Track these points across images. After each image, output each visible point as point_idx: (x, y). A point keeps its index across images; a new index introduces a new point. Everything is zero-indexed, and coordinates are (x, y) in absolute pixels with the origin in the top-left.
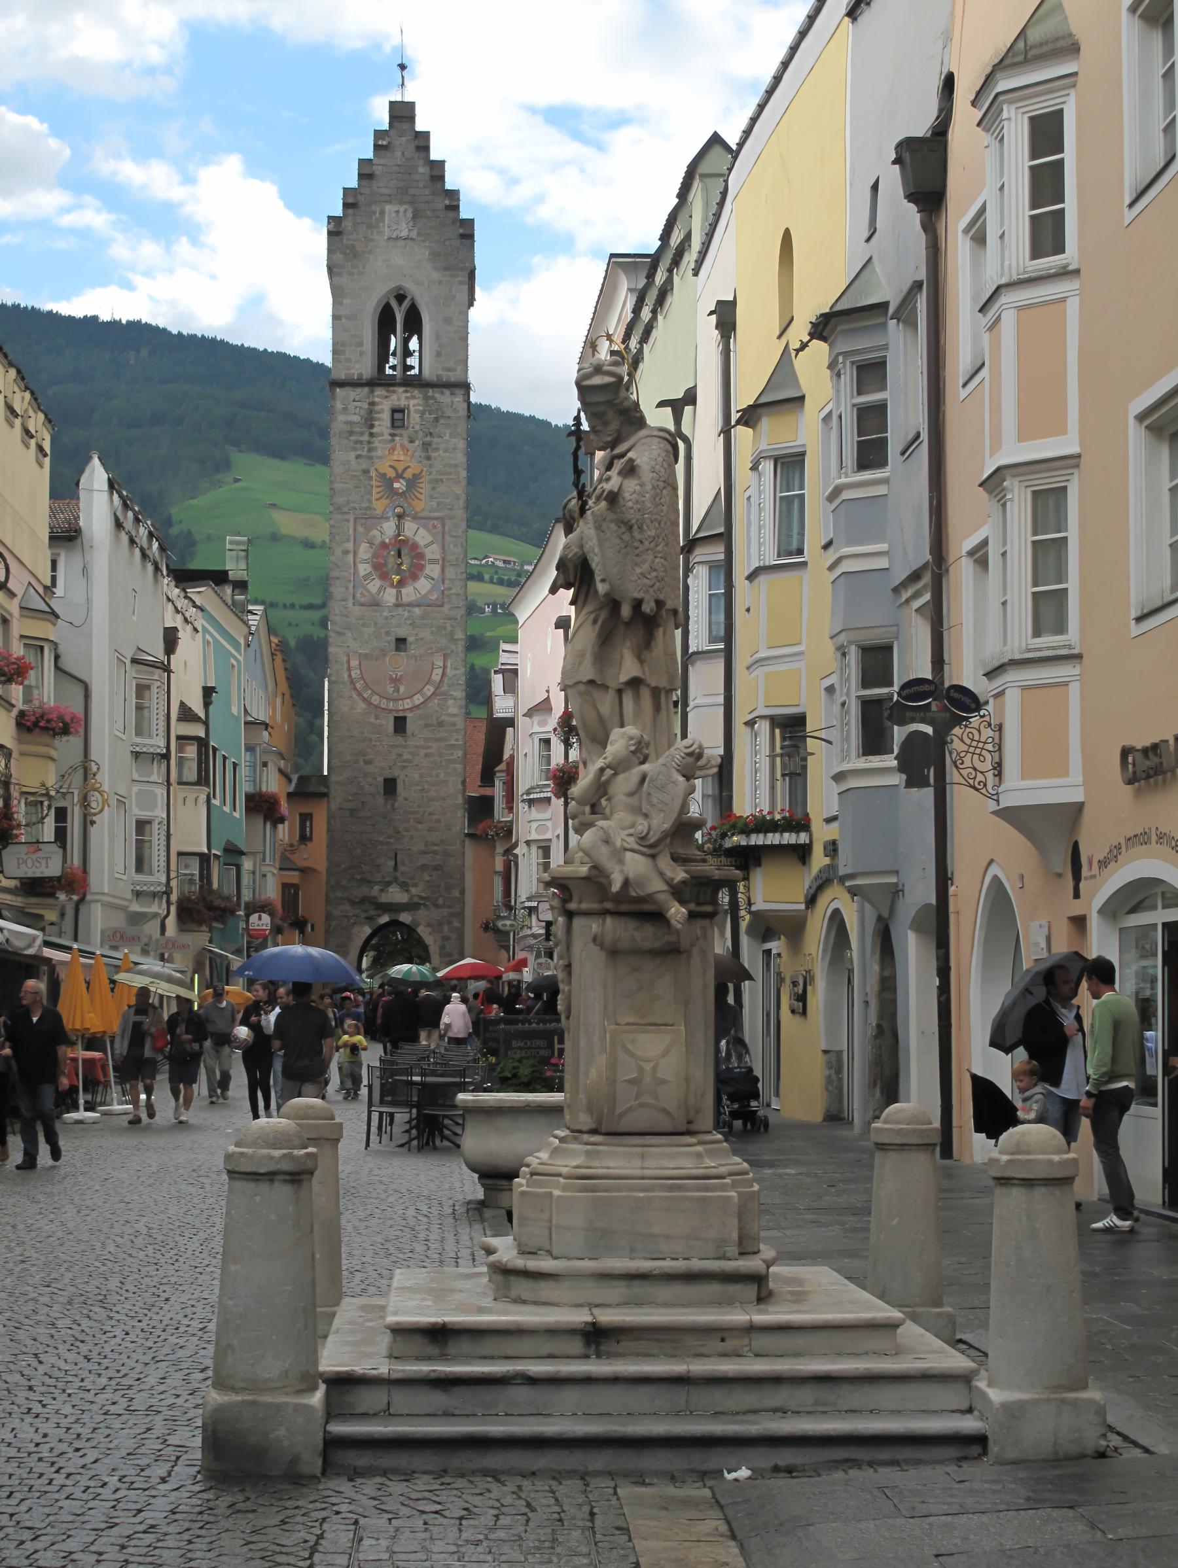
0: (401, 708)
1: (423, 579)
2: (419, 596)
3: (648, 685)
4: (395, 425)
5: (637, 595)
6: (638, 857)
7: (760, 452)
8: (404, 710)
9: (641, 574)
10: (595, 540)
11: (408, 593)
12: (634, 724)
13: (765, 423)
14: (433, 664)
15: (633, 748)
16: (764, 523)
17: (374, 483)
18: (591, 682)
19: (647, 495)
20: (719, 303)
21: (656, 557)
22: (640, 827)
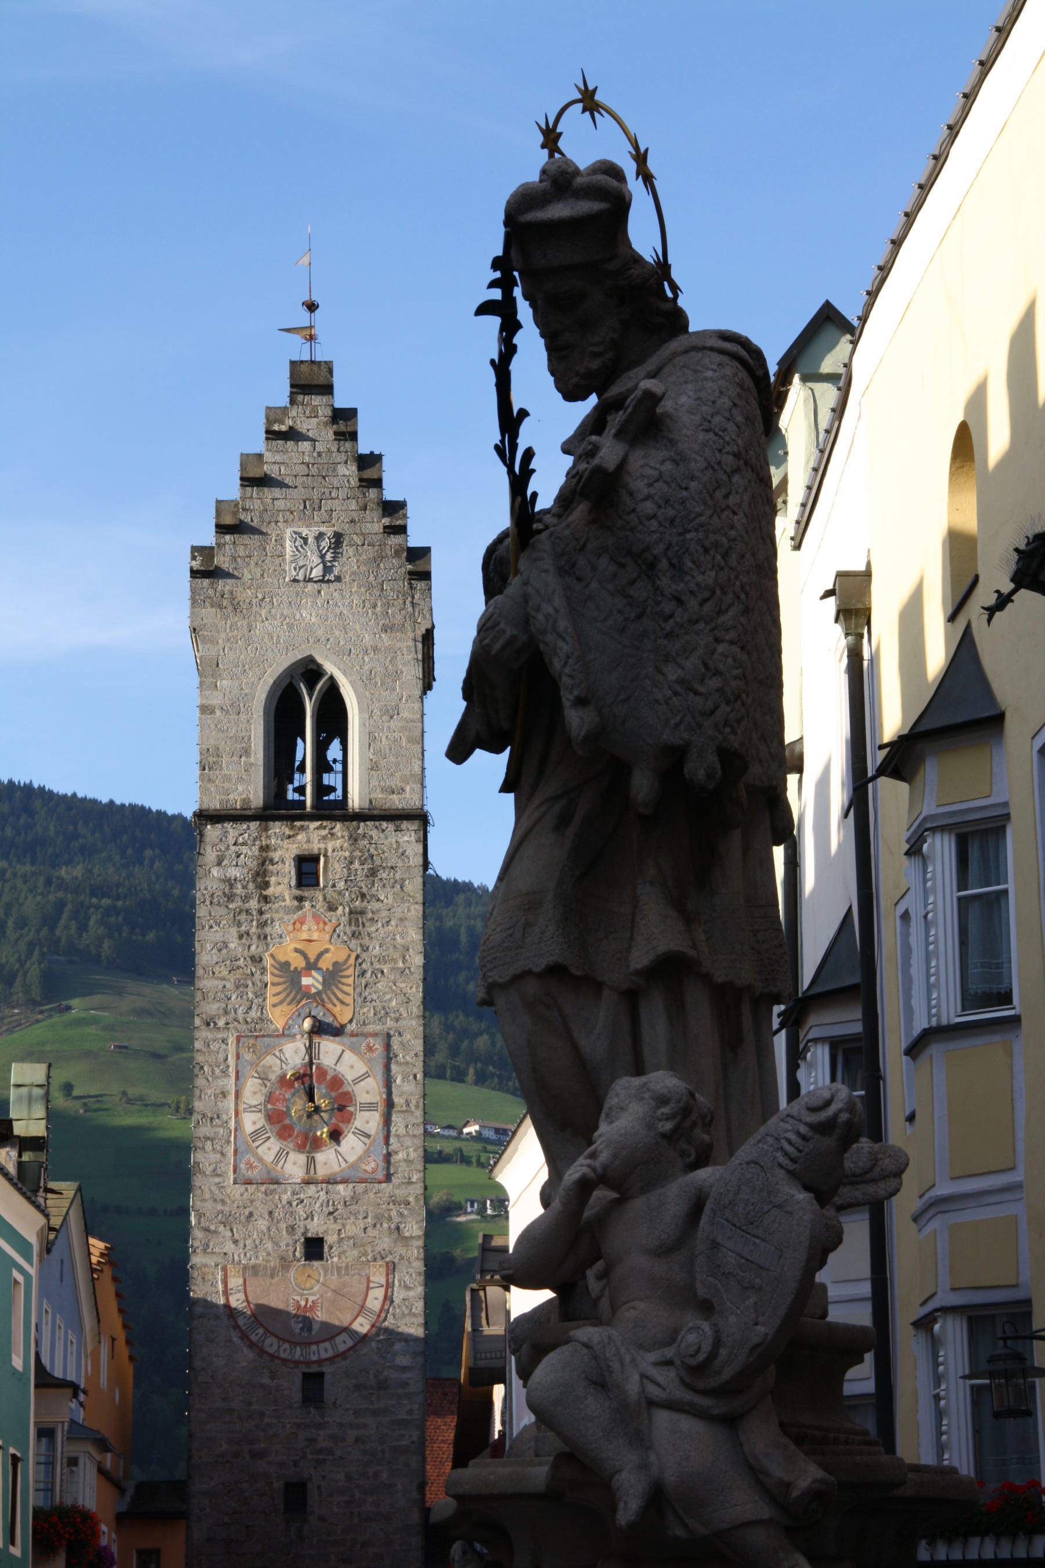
0: (314, 1358)
1: (350, 1135)
2: (343, 1165)
3: (706, 978)
4: (304, 882)
5: (667, 737)
6: (687, 1424)
7: (925, 819)
8: (320, 1362)
9: (681, 681)
10: (558, 601)
11: (328, 1160)
12: (671, 1068)
13: (931, 770)
14: (368, 1279)
15: (668, 1126)
16: (936, 948)
17: (268, 978)
18: (556, 971)
19: (693, 485)
20: (840, 575)
21: (718, 640)
22: (692, 1338)
